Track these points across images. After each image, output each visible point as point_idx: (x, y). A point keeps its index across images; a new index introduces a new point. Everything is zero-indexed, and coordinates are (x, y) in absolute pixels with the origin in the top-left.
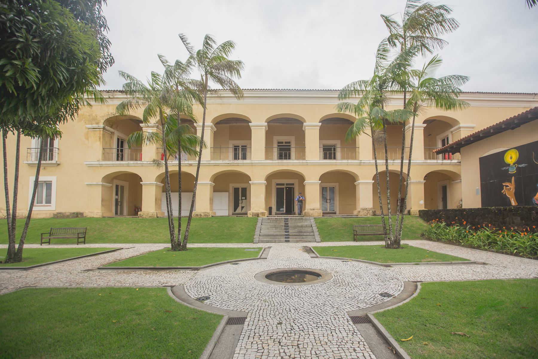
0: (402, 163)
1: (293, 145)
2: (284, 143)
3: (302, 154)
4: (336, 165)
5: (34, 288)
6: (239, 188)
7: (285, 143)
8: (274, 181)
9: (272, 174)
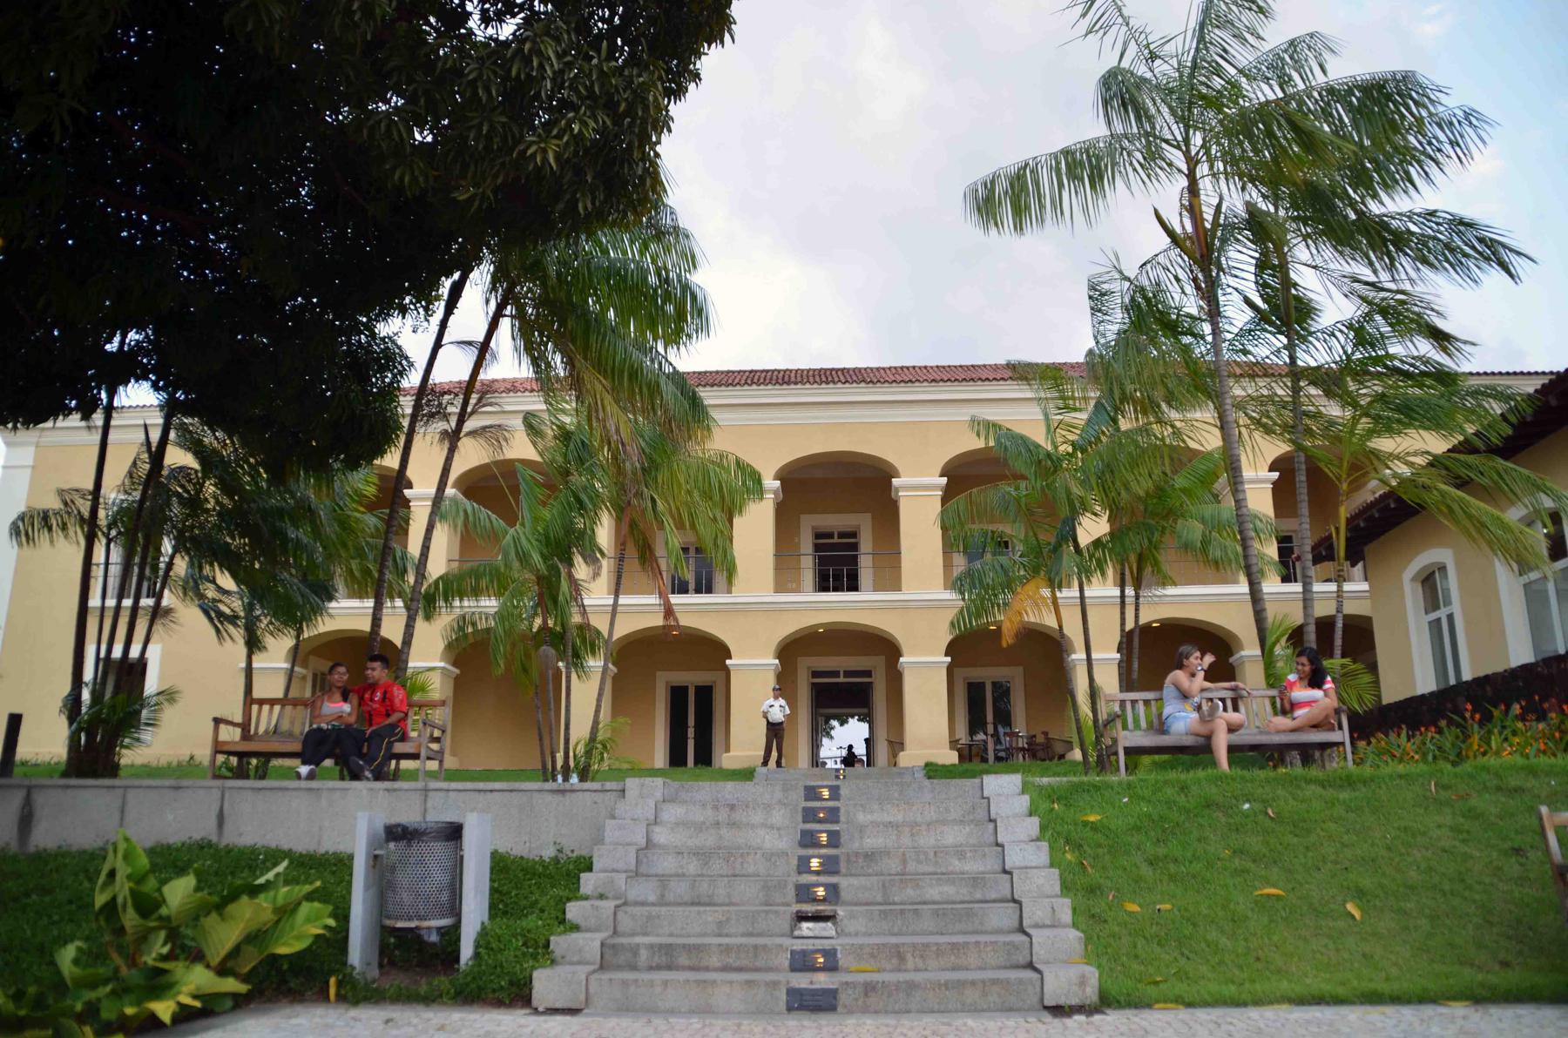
0: (1123, 596)
1: (866, 544)
3: (890, 578)
6: (686, 688)
7: (841, 535)
8: (805, 665)
9: (1202, 627)
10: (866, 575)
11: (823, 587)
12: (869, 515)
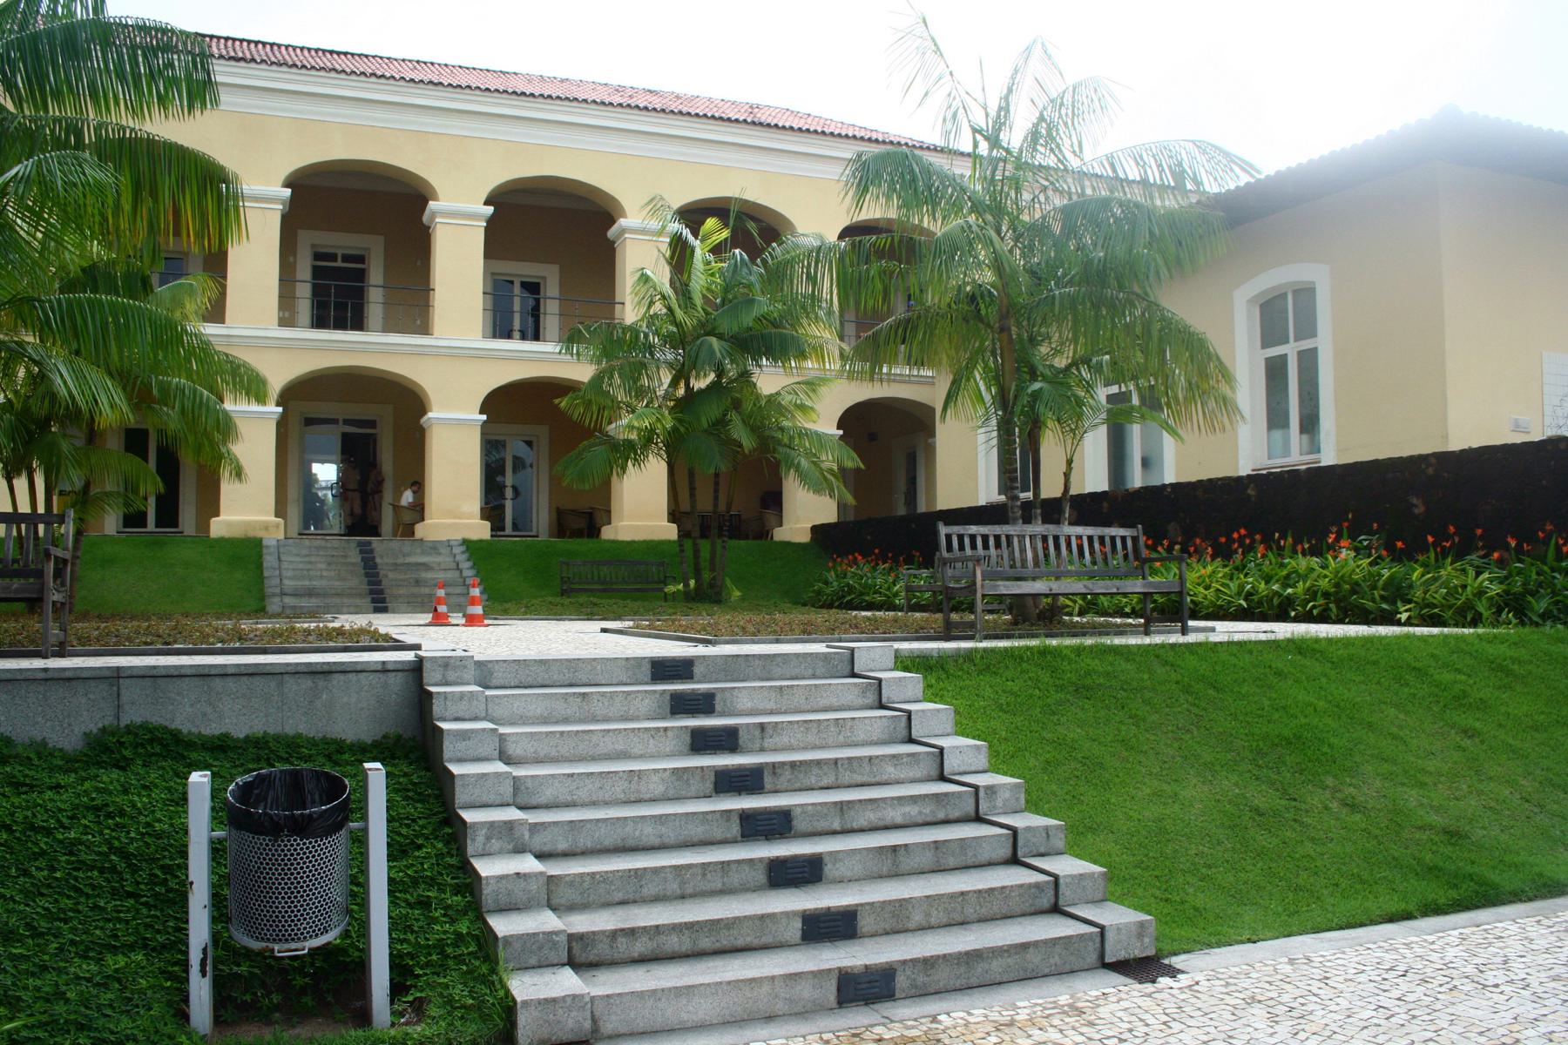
2: (339, 259)
4: (363, 348)
5: (800, 875)
7: (346, 258)
10: (375, 309)
11: (319, 322)
12: (381, 239)
